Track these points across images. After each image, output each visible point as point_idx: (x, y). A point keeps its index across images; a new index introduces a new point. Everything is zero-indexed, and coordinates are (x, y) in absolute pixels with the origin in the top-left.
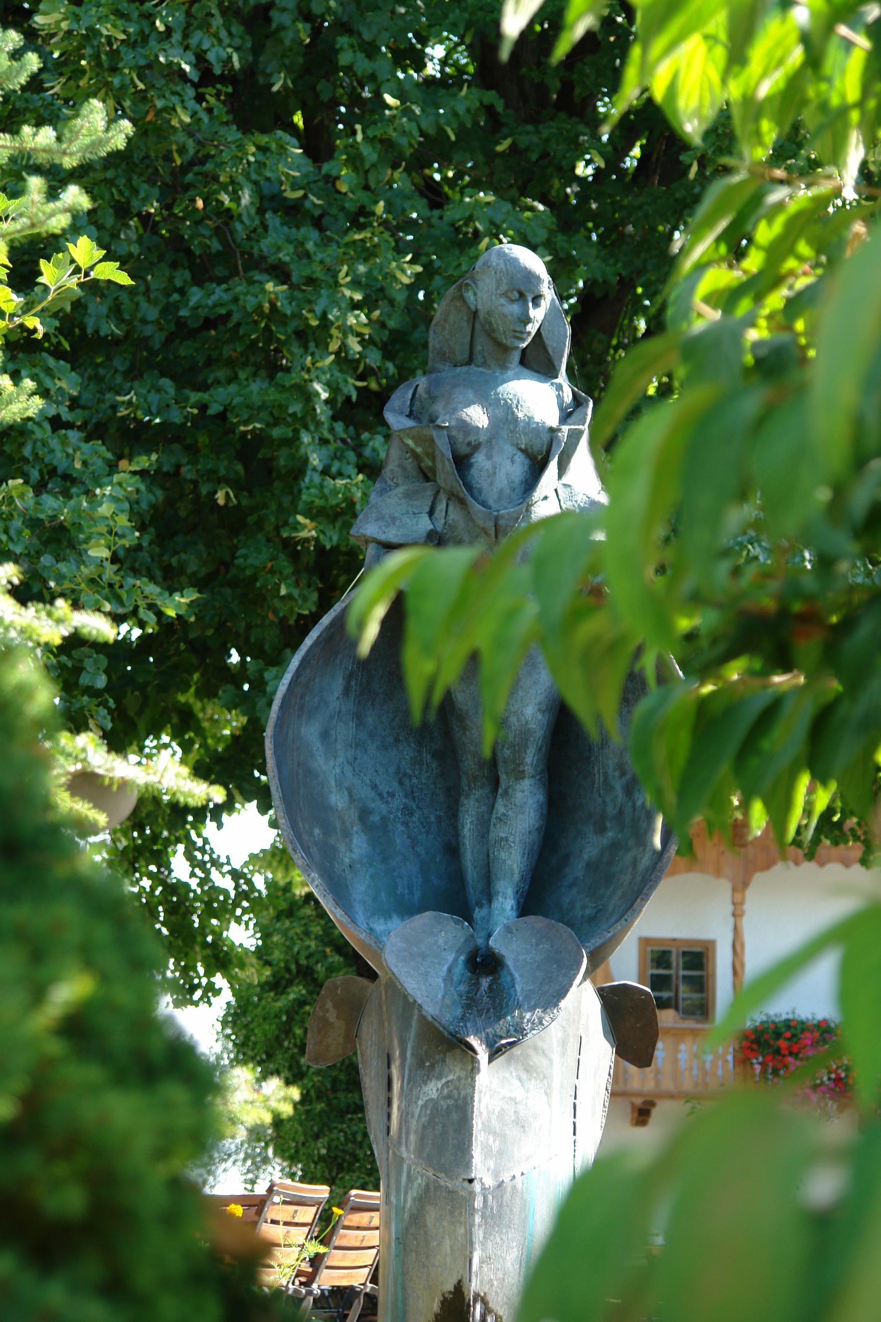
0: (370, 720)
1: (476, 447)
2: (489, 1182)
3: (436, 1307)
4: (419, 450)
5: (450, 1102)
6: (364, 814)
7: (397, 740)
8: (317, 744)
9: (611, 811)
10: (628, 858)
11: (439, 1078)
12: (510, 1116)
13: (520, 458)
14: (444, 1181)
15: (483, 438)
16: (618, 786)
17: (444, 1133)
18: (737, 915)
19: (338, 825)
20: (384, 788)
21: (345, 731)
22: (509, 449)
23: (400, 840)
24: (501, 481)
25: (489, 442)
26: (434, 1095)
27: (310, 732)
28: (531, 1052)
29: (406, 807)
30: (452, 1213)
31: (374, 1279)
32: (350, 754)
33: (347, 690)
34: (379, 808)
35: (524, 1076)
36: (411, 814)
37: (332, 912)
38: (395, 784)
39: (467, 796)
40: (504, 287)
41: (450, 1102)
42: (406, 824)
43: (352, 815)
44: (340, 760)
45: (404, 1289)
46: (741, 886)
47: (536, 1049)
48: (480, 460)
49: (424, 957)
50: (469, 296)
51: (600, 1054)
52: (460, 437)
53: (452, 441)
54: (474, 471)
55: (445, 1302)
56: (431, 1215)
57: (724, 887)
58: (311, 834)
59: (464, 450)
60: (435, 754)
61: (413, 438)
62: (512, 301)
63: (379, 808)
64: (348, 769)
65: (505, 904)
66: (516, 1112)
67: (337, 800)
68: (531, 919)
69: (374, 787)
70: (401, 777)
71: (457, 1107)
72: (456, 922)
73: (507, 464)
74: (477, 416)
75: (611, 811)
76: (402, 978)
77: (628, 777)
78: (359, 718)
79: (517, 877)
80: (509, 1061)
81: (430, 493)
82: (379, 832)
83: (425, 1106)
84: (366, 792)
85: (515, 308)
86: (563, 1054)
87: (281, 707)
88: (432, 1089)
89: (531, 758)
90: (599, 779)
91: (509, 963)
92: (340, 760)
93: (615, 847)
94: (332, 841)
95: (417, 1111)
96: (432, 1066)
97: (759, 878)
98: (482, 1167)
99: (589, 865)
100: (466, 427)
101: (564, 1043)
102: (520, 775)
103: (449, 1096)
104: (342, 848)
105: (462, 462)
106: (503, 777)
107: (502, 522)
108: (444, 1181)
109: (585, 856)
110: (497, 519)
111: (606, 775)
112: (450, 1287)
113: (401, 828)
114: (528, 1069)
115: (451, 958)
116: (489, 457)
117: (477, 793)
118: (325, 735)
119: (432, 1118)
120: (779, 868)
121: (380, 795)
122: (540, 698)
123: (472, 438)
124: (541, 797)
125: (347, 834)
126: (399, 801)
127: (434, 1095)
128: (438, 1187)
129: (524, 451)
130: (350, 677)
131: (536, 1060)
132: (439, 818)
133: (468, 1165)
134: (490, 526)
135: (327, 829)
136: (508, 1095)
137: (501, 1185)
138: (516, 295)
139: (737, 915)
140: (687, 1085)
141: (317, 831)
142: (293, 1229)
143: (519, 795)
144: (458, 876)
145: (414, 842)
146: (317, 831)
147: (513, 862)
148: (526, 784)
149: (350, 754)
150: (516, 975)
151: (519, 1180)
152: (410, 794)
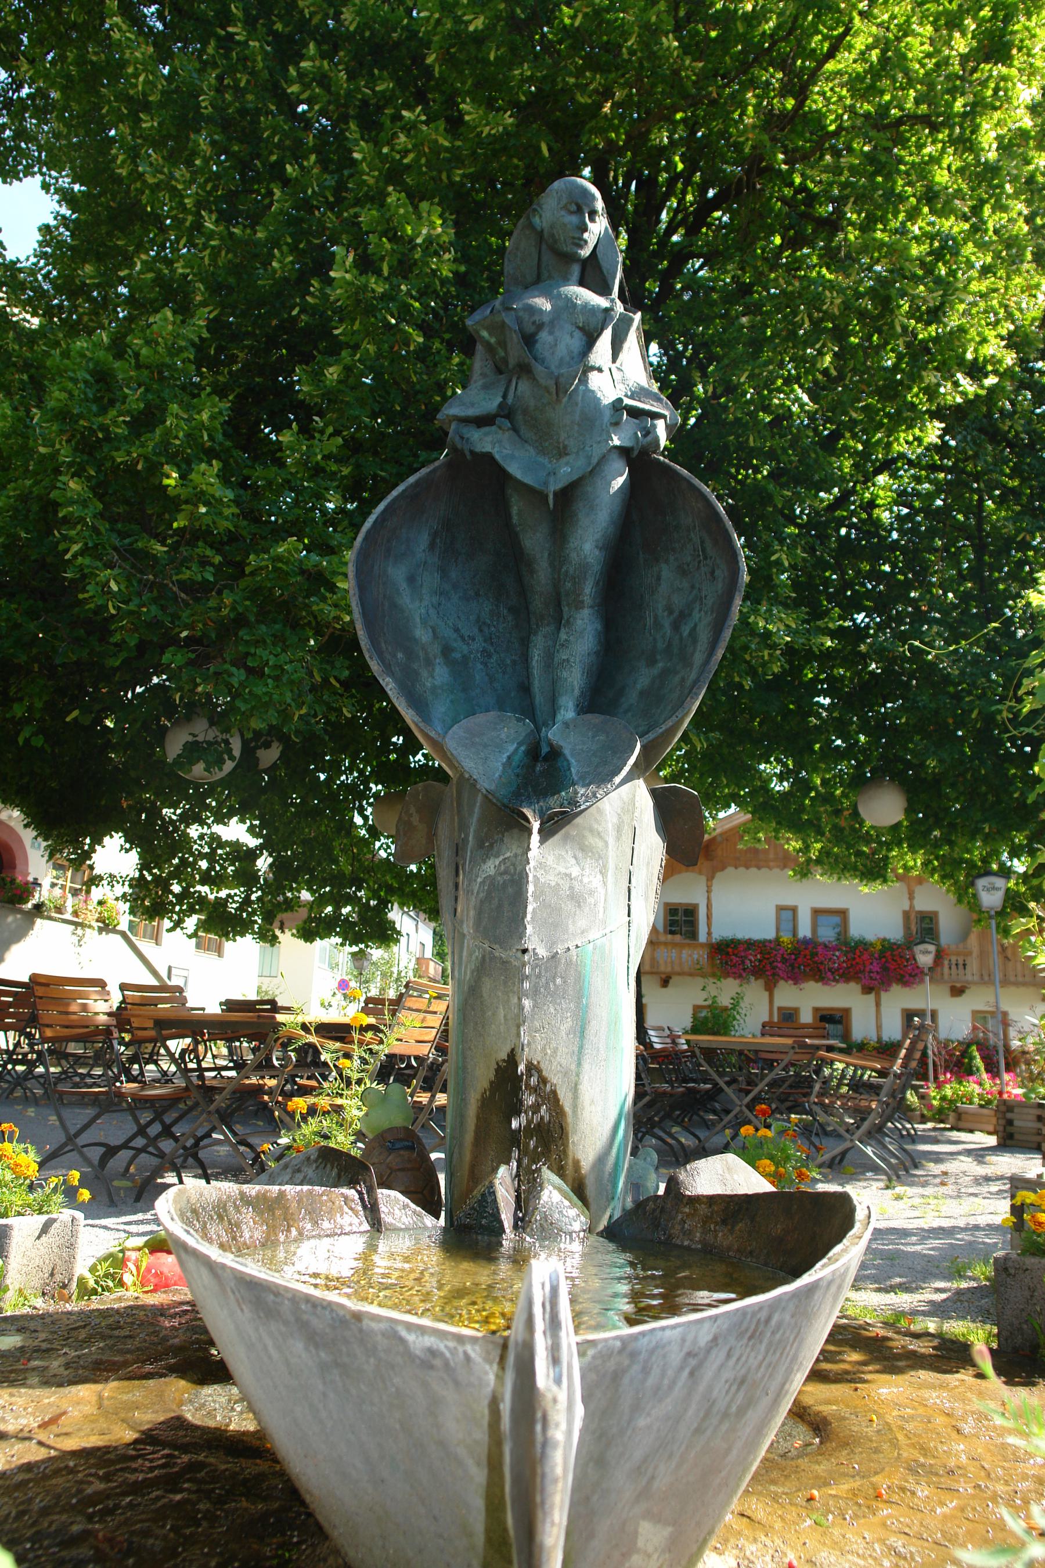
0: (453, 575)
1: (540, 327)
2: (542, 952)
3: (491, 1075)
4: (493, 340)
5: (507, 877)
6: (446, 651)
7: (477, 594)
8: (403, 585)
9: (661, 645)
10: (677, 679)
11: (497, 856)
12: (565, 890)
13: (578, 334)
14: (499, 953)
15: (546, 319)
16: (667, 624)
17: (500, 906)
18: (709, 892)
19: (421, 654)
20: (466, 632)
21: (430, 580)
22: (568, 327)
23: (479, 676)
24: (562, 350)
25: (552, 322)
26: (492, 871)
27: (398, 573)
28: (587, 834)
29: (484, 650)
30: (505, 983)
31: (441, 1050)
32: (435, 599)
33: (432, 546)
34: (461, 649)
35: (580, 855)
36: (490, 656)
37: (421, 731)
38: (476, 630)
39: (536, 634)
40: (564, 201)
41: (507, 877)
42: (485, 664)
43: (435, 649)
44: (425, 603)
45: (464, 1058)
46: (710, 878)
47: (591, 830)
48: (544, 336)
49: (485, 746)
50: (536, 220)
51: (652, 847)
52: (526, 317)
53: (519, 321)
54: (538, 346)
55: (499, 1070)
56: (487, 985)
57: (703, 879)
58: (395, 656)
59: (530, 329)
60: (511, 610)
61: (487, 329)
62: (572, 213)
63: (461, 649)
64: (432, 611)
65: (567, 712)
66: (571, 888)
67: (422, 634)
68: (589, 716)
69: (457, 630)
70: (481, 625)
71: (512, 881)
72: (518, 720)
73: (567, 339)
74: (544, 304)
75: (661, 645)
76: (461, 758)
77: (676, 614)
78: (443, 571)
79: (577, 692)
80: (566, 838)
81: (503, 383)
82: (459, 668)
83: (483, 883)
84: (448, 633)
85: (574, 219)
86: (618, 838)
87: (365, 539)
88: (490, 867)
89: (588, 590)
90: (649, 621)
91: (567, 752)
92: (425, 603)
93: (665, 674)
94: (415, 666)
95: (476, 889)
96: (491, 846)
97: (719, 875)
98: (534, 940)
99: (642, 693)
100: (532, 310)
101: (619, 829)
102: (579, 605)
103: (505, 872)
104: (425, 673)
105: (529, 340)
106: (565, 609)
107: (562, 380)
108: (499, 953)
109: (639, 686)
110: (557, 379)
111: (656, 617)
112: (503, 1055)
113: (479, 666)
114: (583, 848)
115: (511, 748)
116: (551, 333)
117: (545, 630)
118: (411, 579)
119: (489, 892)
120: (730, 870)
121: (462, 637)
122: (597, 536)
123: (537, 318)
124: (599, 626)
125: (429, 663)
126: (478, 645)
127: (492, 871)
128: (493, 958)
129: (581, 329)
130: (434, 535)
131: (592, 840)
132: (514, 662)
133: (522, 935)
134: (551, 384)
135: (410, 655)
136: (563, 870)
137: (554, 956)
138: (574, 208)
139: (709, 892)
140: (686, 969)
141: (400, 655)
142: (429, 1016)
143: (579, 622)
144: (525, 689)
145: (492, 679)
146: (400, 655)
147: (574, 679)
148: (586, 612)
149: (435, 599)
150: (573, 761)
151: (573, 952)
152: (489, 640)
